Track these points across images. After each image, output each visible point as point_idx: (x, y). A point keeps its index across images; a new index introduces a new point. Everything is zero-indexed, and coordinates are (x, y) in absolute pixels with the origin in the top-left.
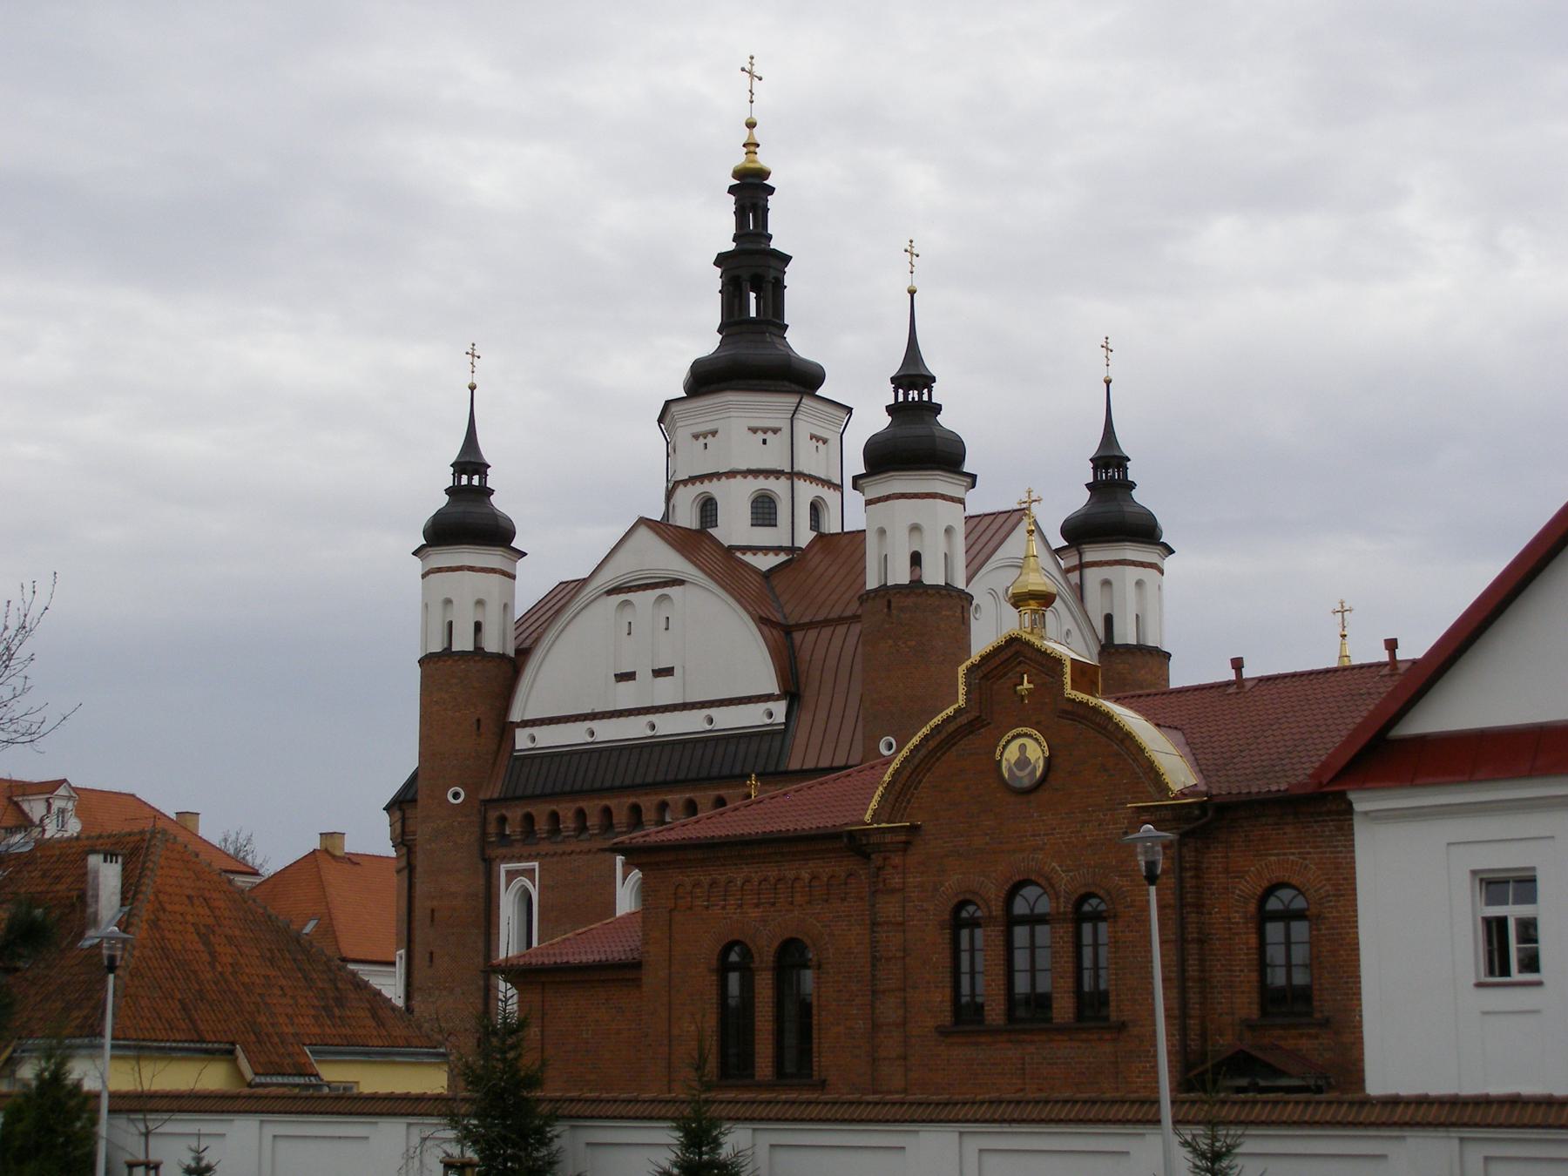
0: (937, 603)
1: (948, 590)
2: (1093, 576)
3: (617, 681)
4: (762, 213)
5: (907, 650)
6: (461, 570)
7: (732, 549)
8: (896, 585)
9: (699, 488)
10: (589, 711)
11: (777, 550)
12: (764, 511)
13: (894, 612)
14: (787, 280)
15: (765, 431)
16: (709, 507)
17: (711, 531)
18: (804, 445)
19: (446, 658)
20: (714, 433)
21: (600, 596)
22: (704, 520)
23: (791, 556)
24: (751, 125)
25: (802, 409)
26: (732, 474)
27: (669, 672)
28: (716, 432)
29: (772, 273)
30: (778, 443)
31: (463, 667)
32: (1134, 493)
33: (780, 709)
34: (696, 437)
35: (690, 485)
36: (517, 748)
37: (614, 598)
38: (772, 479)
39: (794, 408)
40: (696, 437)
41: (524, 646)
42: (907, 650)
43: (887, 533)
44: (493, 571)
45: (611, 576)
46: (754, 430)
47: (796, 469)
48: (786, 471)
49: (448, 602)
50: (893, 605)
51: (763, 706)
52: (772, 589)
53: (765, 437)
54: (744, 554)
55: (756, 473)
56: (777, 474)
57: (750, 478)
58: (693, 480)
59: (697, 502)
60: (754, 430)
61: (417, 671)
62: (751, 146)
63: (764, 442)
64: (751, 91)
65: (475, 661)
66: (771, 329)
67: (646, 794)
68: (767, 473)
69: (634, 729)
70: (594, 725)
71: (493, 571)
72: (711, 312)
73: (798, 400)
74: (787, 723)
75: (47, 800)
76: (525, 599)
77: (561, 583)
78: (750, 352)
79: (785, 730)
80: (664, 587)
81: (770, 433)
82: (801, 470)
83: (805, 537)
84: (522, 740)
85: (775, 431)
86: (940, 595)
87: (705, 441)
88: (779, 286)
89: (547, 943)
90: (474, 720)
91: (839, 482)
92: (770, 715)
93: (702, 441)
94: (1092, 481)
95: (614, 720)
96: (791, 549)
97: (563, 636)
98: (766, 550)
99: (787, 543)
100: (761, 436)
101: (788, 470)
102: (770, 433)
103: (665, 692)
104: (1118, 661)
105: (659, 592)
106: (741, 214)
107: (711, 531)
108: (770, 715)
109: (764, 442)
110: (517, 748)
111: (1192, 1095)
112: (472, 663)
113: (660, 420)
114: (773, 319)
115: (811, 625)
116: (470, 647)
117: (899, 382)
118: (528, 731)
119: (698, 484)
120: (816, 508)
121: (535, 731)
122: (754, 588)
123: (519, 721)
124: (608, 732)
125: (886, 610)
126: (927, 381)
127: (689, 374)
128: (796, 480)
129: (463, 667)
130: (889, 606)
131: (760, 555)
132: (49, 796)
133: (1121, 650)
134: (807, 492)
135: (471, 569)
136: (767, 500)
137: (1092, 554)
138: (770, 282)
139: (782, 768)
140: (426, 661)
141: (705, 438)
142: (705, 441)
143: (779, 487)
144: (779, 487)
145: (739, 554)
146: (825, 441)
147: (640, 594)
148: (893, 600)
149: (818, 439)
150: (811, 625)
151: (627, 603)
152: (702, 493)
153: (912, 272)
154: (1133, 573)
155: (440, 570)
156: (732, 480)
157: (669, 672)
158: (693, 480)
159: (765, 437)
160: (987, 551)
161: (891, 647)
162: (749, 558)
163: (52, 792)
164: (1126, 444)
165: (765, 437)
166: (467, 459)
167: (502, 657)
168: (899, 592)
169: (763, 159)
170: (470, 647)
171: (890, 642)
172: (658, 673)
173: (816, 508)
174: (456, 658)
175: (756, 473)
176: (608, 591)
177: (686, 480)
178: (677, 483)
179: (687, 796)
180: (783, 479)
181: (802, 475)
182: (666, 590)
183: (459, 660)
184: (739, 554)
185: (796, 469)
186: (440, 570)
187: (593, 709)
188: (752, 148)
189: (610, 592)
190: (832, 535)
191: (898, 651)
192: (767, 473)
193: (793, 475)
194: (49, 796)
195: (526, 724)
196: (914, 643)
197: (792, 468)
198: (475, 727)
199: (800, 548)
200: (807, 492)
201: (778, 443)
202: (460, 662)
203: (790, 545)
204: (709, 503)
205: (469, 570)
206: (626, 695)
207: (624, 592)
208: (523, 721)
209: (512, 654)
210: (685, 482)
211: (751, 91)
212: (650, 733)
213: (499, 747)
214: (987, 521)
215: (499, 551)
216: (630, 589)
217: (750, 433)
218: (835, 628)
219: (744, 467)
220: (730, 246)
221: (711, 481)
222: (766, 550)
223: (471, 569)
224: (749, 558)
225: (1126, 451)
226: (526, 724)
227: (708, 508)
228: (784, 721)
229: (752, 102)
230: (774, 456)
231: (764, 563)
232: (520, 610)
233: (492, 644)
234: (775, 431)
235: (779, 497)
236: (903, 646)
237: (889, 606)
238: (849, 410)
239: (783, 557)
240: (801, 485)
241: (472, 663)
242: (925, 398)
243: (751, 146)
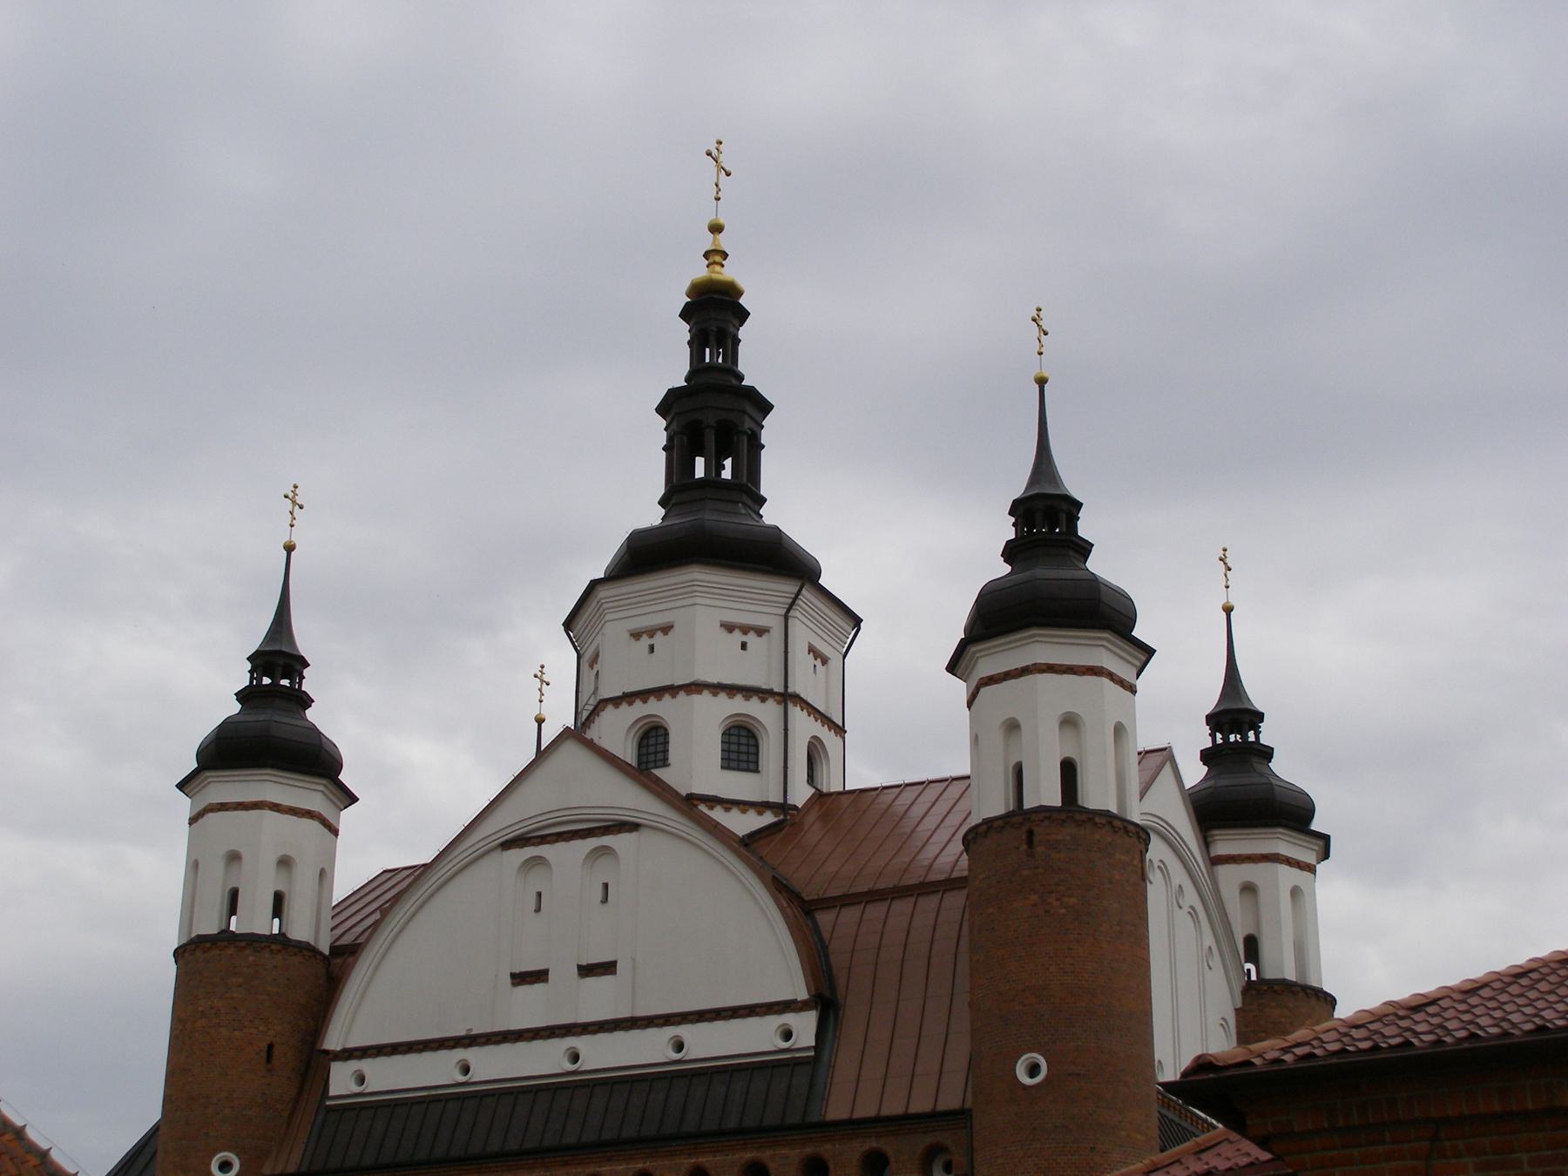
0: (1109, 839)
1: (1114, 823)
3: (514, 984)
4: (730, 344)
5: (1063, 911)
6: (260, 808)
8: (1041, 806)
9: (639, 710)
10: (463, 1033)
11: (761, 807)
13: (1039, 849)
14: (765, 436)
15: (745, 630)
16: (652, 741)
17: (658, 772)
18: (801, 662)
19: (225, 943)
20: (666, 629)
21: (495, 848)
22: (644, 759)
23: (782, 817)
24: (716, 229)
25: (798, 605)
26: (695, 687)
27: (608, 968)
28: (672, 627)
29: (748, 424)
31: (251, 958)
32: (1274, 765)
33: (805, 1027)
34: (636, 635)
35: (624, 706)
36: (331, 1094)
38: (755, 701)
39: (790, 600)
40: (636, 635)
41: (347, 939)
42: (1063, 911)
43: (1023, 728)
44: (309, 814)
45: (506, 821)
46: (729, 628)
47: (790, 690)
48: (776, 690)
49: (234, 857)
50: (1036, 839)
51: (774, 1022)
53: (745, 640)
54: (711, 808)
55: (732, 690)
56: (763, 694)
57: (722, 696)
59: (632, 734)
60: (729, 628)
62: (715, 256)
63: (744, 646)
64: (717, 185)
65: (271, 951)
66: (745, 498)
67: (566, 1164)
68: (748, 692)
69: (545, 1060)
70: (471, 1055)
71: (309, 814)
72: (655, 481)
73: (795, 589)
74: (818, 1047)
76: (348, 876)
77: (385, 872)
79: (816, 1060)
80: (603, 834)
81: (659, 635)
82: (798, 692)
83: (800, 794)
84: (341, 1080)
85: (761, 632)
86: (1113, 827)
87: (651, 641)
88: (756, 446)
90: (264, 1045)
91: (841, 724)
92: (787, 1035)
93: (645, 641)
94: (1211, 745)
95: (506, 1047)
96: (783, 808)
97: (421, 916)
98: (743, 806)
99: (775, 797)
101: (779, 688)
102: (659, 635)
103: (599, 999)
104: (1273, 1004)
105: (593, 842)
106: (698, 343)
107: (658, 772)
108: (787, 1035)
109: (744, 646)
110: (331, 1094)
112: (267, 954)
113: (568, 625)
115: (847, 900)
117: (1216, 721)
118: (354, 1065)
120: (815, 753)
121: (366, 1066)
123: (338, 1049)
124: (492, 1065)
125: (1024, 847)
126: (1254, 718)
127: (625, 548)
128: (790, 706)
129: (251, 958)
130: (1030, 842)
131: (735, 812)
133: (1276, 988)
135: (276, 807)
136: (743, 733)
138: (745, 432)
139: (814, 1118)
140: (191, 952)
141: (651, 636)
142: (651, 641)
143: (765, 714)
144: (765, 714)
146: (825, 661)
147: (561, 846)
148: (1035, 829)
149: (745, 630)
150: (847, 900)
151: (538, 861)
152: (645, 717)
153: (1040, 354)
154: (1287, 876)
155: (223, 807)
156: (695, 697)
157: (608, 968)
159: (744, 639)
161: (1035, 905)
164: (1257, 693)
165: (744, 639)
166: (276, 648)
168: (1049, 818)
169: (729, 272)
171: (1034, 898)
172: (587, 971)
173: (815, 753)
174: (243, 944)
175: (732, 690)
176: (507, 841)
177: (618, 698)
178: (602, 704)
179: (640, 1166)
182: (607, 840)
183: (244, 948)
184: (703, 808)
185: (790, 690)
186: (223, 807)
187: (471, 1030)
188: (718, 259)
189: (507, 845)
190: (831, 794)
191: (1046, 912)
192: (748, 692)
195: (348, 1054)
196: (1073, 900)
197: (786, 687)
198: (264, 1054)
202: (247, 952)
203: (782, 801)
204: (653, 733)
205: (271, 809)
206: (529, 1008)
207: (533, 845)
208: (345, 1050)
210: (616, 701)
211: (717, 185)
212: (570, 1067)
213: (300, 1094)
215: (320, 784)
216: (543, 840)
217: (724, 633)
218: (891, 903)
219: (714, 680)
220: (742, 301)
221: (659, 698)
222: (743, 806)
223: (276, 807)
224: (717, 814)
225: (1258, 704)
226: (348, 1054)
227: (653, 741)
228: (814, 1044)
229: (718, 199)
230: (756, 668)
232: (343, 887)
233: (300, 930)
234: (761, 632)
235: (763, 726)
236: (1056, 904)
237: (1030, 842)
239: (768, 818)
240: (797, 714)
241: (267, 954)
243: (715, 256)
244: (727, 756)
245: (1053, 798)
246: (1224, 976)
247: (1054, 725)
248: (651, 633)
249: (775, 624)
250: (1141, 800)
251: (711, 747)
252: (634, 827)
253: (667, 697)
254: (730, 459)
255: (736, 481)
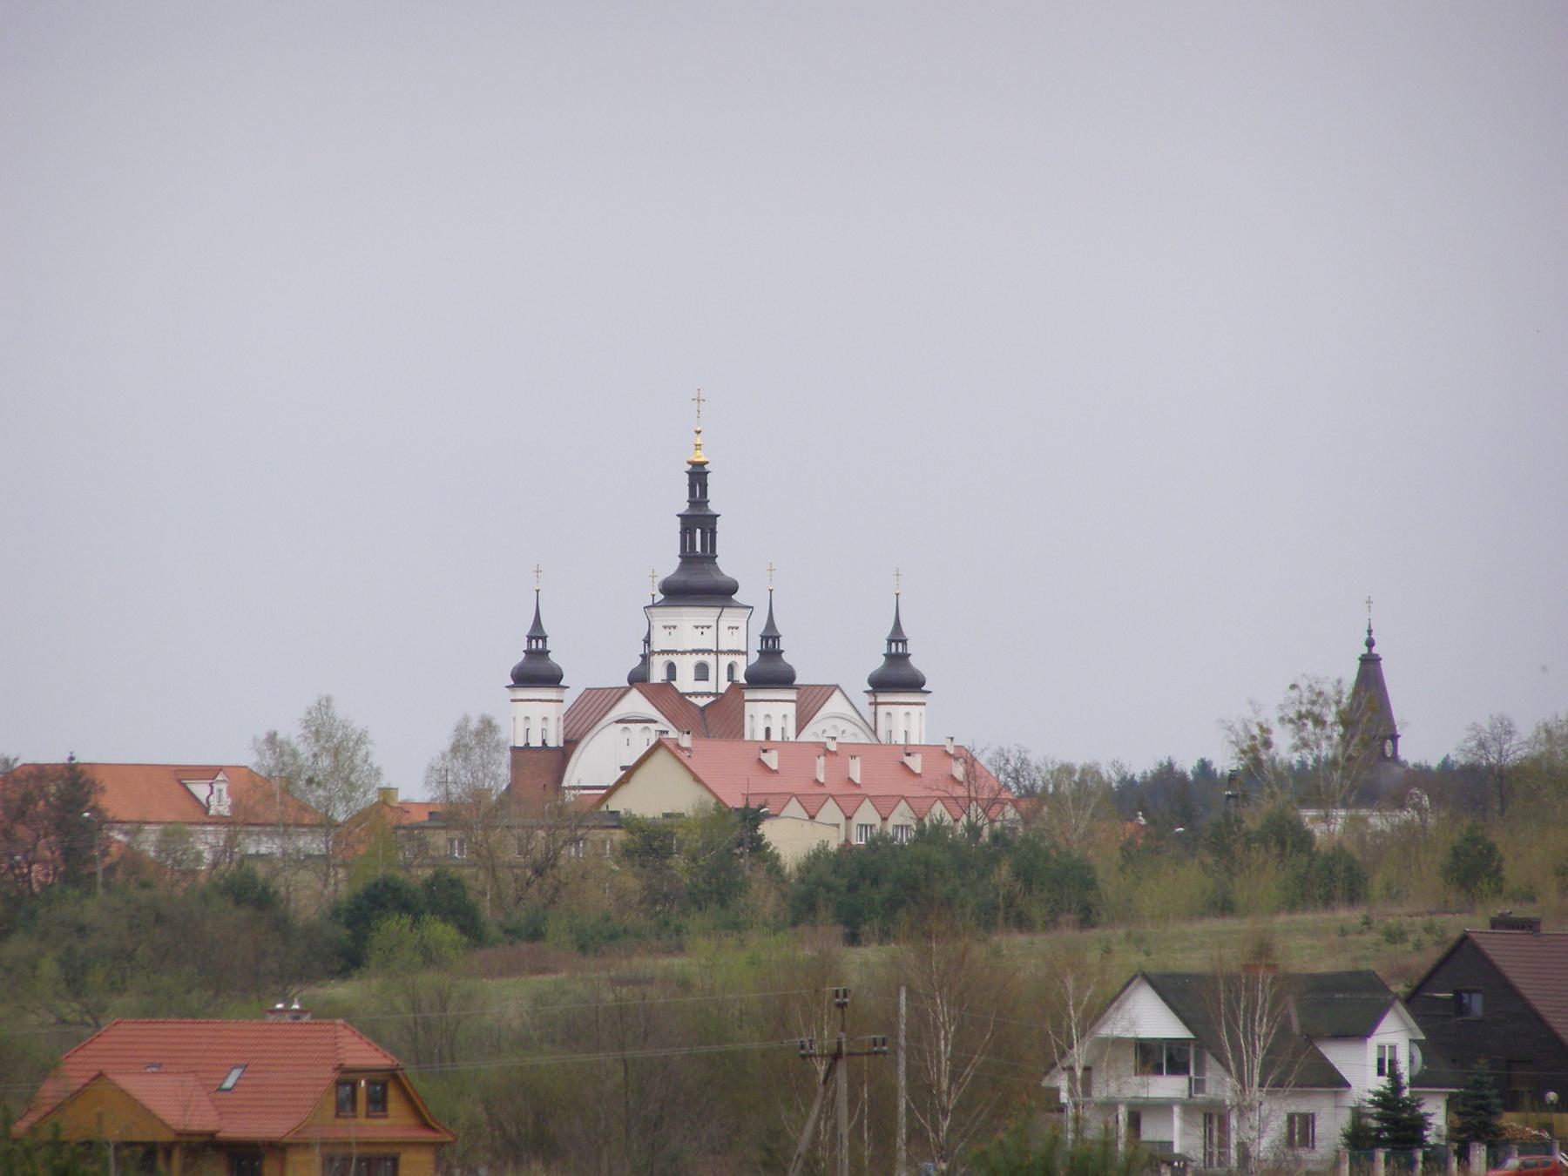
2: (882, 710)
7: (683, 695)
11: (708, 694)
12: (702, 672)
15: (703, 627)
17: (672, 682)
26: (684, 653)
30: (710, 633)
37: (619, 725)
49: (527, 718)
52: (704, 719)
56: (709, 652)
57: (694, 654)
58: (663, 652)
61: (52, 753)
63: (670, 633)
75: (211, 785)
78: (697, 579)
81: (705, 628)
83: (724, 686)
85: (708, 627)
89: (902, 1041)
96: (716, 694)
99: (714, 691)
100: (700, 630)
101: (715, 649)
102: (705, 628)
105: (624, 725)
107: (672, 682)
109: (670, 633)
111: (904, 1008)
114: (709, 557)
116: (780, 739)
119: (700, 654)
122: (577, 726)
131: (699, 698)
132: (211, 781)
134: (725, 660)
135: (540, 700)
137: (881, 698)
143: (710, 659)
144: (710, 659)
145: (687, 697)
158: (663, 652)
160: (819, 705)
162: (693, 699)
163: (214, 779)
167: (557, 749)
170: (780, 739)
180: (712, 654)
181: (723, 652)
184: (687, 697)
185: (720, 648)
189: (617, 722)
193: (718, 652)
194: (211, 781)
197: (876, 709)
199: (721, 694)
200: (725, 660)
201: (710, 633)
209: (561, 745)
214: (615, 691)
217: (695, 630)
219: (690, 649)
224: (693, 699)
231: (701, 702)
233: (552, 743)
234: (708, 627)
238: (752, 608)
239: (712, 699)
242: (540, 646)
244: (873, 700)
245: (746, 698)
246: (134, 763)
247: (903, 713)
248: (703, 627)
249: (714, 625)
250: (568, 687)
251: (691, 673)
252: (655, 722)
253: (675, 655)
254: (1424, 1038)
255: (704, 554)
